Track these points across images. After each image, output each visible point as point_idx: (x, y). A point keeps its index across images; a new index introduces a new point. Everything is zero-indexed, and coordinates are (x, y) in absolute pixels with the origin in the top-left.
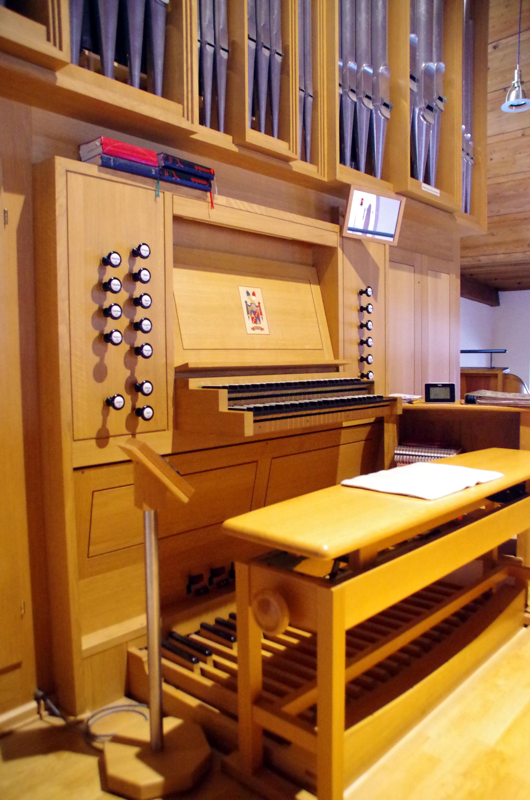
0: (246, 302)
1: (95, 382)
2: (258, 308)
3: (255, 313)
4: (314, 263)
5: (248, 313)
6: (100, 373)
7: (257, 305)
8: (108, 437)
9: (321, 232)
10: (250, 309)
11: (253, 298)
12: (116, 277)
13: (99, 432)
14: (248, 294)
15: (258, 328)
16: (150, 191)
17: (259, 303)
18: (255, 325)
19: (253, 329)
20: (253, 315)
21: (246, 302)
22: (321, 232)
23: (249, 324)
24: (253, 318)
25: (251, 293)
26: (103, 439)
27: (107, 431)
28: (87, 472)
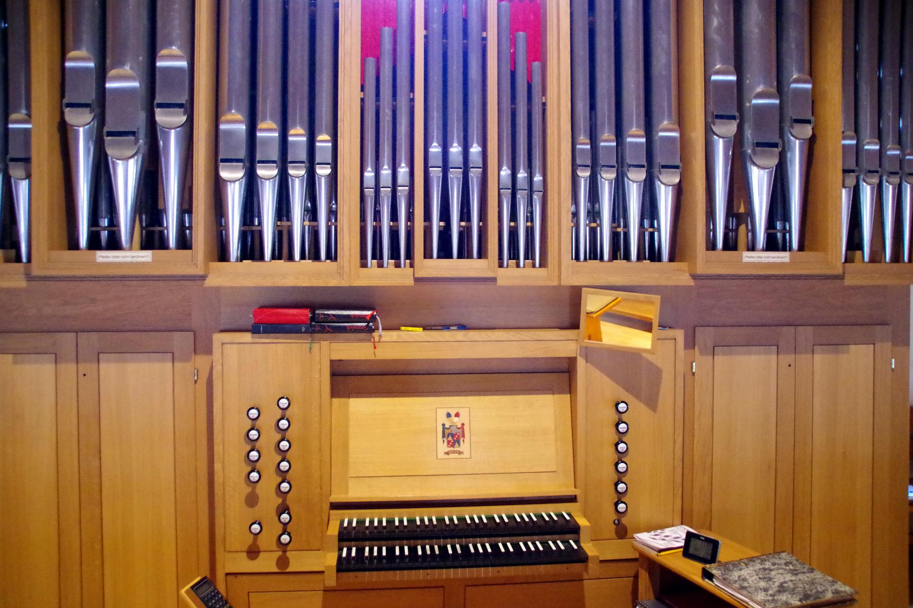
0: (443, 425)
1: (244, 506)
2: (460, 431)
3: (453, 436)
4: (559, 375)
5: (444, 436)
6: (252, 500)
7: (459, 426)
8: (259, 552)
9: (558, 344)
10: (447, 432)
11: (456, 419)
12: (267, 422)
13: (250, 547)
14: (449, 415)
15: (454, 452)
16: (304, 345)
17: (463, 424)
18: (452, 449)
19: (447, 453)
20: (450, 438)
21: (443, 425)
22: (558, 344)
23: (443, 447)
24: (449, 442)
25: (453, 415)
26: (253, 553)
28: (239, 577)
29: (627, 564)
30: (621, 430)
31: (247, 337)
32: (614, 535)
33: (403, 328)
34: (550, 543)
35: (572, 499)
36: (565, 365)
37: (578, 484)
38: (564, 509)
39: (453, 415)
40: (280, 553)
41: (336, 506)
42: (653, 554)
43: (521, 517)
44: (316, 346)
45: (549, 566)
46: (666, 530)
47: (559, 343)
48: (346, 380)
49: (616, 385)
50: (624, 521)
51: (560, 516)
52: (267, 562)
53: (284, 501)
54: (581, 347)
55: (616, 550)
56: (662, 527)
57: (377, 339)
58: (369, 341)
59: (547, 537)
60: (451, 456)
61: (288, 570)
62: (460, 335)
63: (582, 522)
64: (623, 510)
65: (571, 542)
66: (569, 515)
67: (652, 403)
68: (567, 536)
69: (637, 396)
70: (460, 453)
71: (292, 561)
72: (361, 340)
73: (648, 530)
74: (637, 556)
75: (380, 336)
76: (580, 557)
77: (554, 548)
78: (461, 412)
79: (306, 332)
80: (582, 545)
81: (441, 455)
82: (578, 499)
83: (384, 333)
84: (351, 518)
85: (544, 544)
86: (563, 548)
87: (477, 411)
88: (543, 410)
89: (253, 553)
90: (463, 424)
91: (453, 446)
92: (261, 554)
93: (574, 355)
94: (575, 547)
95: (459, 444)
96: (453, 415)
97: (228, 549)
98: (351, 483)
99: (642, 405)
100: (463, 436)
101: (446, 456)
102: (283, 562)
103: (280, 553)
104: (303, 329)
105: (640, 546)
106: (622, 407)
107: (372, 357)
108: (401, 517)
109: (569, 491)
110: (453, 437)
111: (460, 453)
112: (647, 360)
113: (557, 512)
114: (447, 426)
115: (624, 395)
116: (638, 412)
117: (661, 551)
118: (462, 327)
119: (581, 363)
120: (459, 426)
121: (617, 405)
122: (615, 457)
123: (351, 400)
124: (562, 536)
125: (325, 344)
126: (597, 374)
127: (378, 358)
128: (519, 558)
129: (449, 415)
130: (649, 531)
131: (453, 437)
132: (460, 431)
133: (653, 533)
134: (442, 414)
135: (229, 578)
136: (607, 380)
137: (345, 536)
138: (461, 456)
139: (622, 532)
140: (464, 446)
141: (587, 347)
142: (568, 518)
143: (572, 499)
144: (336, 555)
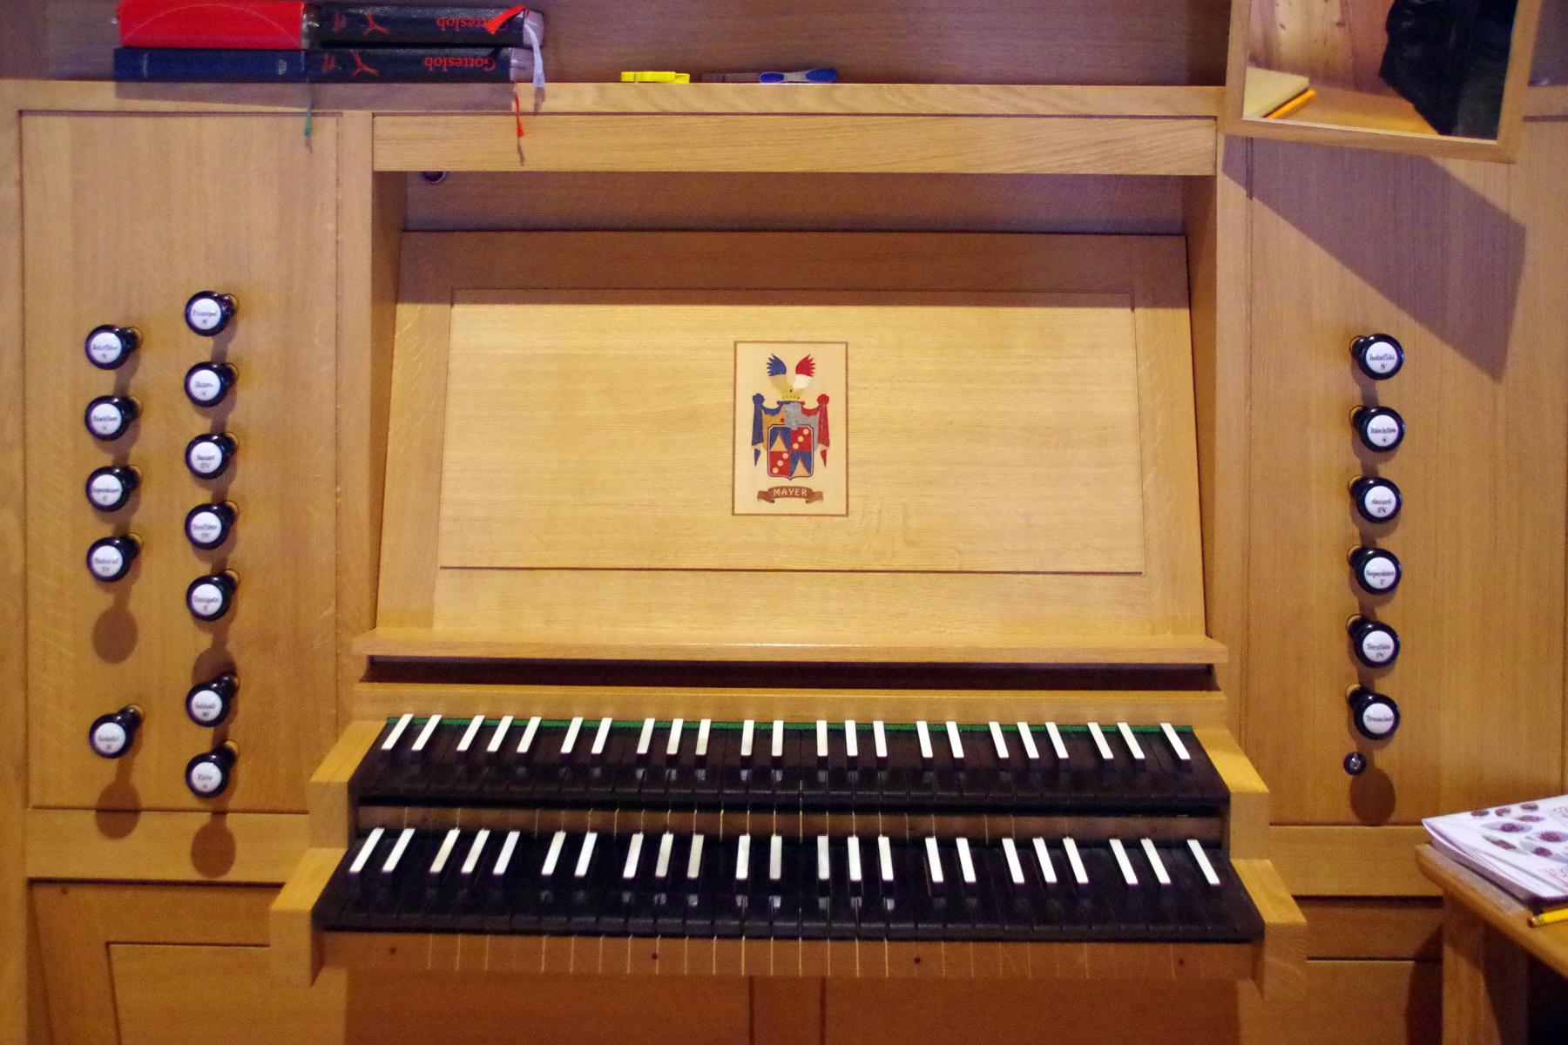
0: (758, 399)
3: (789, 435)
4: (1152, 244)
5: (757, 437)
6: (115, 637)
8: (136, 811)
10: (769, 421)
11: (801, 381)
13: (108, 792)
14: (777, 367)
15: (790, 493)
17: (824, 400)
18: (783, 481)
19: (767, 496)
20: (779, 446)
21: (758, 399)
23: (754, 474)
24: (774, 457)
26: (118, 813)
27: (133, 794)
28: (75, 893)
29: (1392, 914)
30: (1376, 439)
31: (104, 94)
32: (1346, 811)
33: (627, 76)
34: (1117, 846)
35: (1197, 678)
36: (1169, 209)
37: (1217, 622)
38: (1167, 711)
39: (791, 367)
40: (205, 818)
41: (385, 670)
42: (1512, 914)
43: (1013, 737)
44: (327, 126)
45: (1111, 948)
46: (1545, 806)
47: (1155, 125)
48: (437, 241)
49: (1354, 281)
50: (1383, 758)
51: (1152, 738)
52: (160, 848)
53: (219, 642)
54: (1231, 140)
55: (1355, 862)
56: (1531, 792)
57: (527, 104)
58: (504, 110)
59: (1110, 823)
60: (782, 505)
61: (231, 876)
62: (805, 94)
63: (1237, 773)
64: (1385, 727)
65: (1195, 846)
66: (1187, 736)
67: (1486, 346)
68: (1184, 823)
69: (1428, 314)
70: (811, 496)
71: (241, 848)
72: (475, 108)
73: (1476, 801)
74: (1433, 890)
75: (540, 93)
76: (1222, 916)
77: (1131, 878)
78: (820, 357)
79: (285, 79)
80: (1239, 864)
81: (747, 501)
82: (1220, 677)
83: (551, 88)
84: (417, 714)
85: (1096, 853)
86: (1163, 877)
87: (876, 356)
88: (1094, 361)
89: (118, 813)
90: (824, 400)
91: (787, 471)
92: (145, 820)
93: (1206, 171)
94: (1213, 878)
95: (809, 468)
96: (791, 367)
97: (35, 801)
98: (446, 590)
99: (1449, 351)
100: (824, 439)
101: (765, 506)
102: (213, 847)
103: (205, 818)
104: (282, 69)
105: (1450, 870)
106: (1380, 355)
107: (511, 164)
108: (586, 718)
109: (1182, 644)
110: (791, 441)
111: (811, 496)
112: (1469, 194)
113: (1145, 723)
114: (770, 404)
115: (1381, 312)
116: (1433, 378)
117: (1538, 904)
118: (827, 73)
119: (1230, 198)
120: (812, 404)
121: (1358, 351)
122: (1348, 533)
123: (459, 311)
124: (1161, 823)
125: (356, 119)
126: (1286, 236)
127: (531, 165)
128: (996, 908)
129: (777, 367)
130: (1478, 810)
131: (791, 441)
132: (814, 420)
133: (1492, 816)
134: (753, 365)
135: (41, 893)
136: (1319, 261)
137: (384, 784)
138: (815, 507)
139: (1374, 798)
140: (825, 475)
141: (1250, 141)
142: (1183, 754)
143: (1197, 678)
144: (339, 853)
